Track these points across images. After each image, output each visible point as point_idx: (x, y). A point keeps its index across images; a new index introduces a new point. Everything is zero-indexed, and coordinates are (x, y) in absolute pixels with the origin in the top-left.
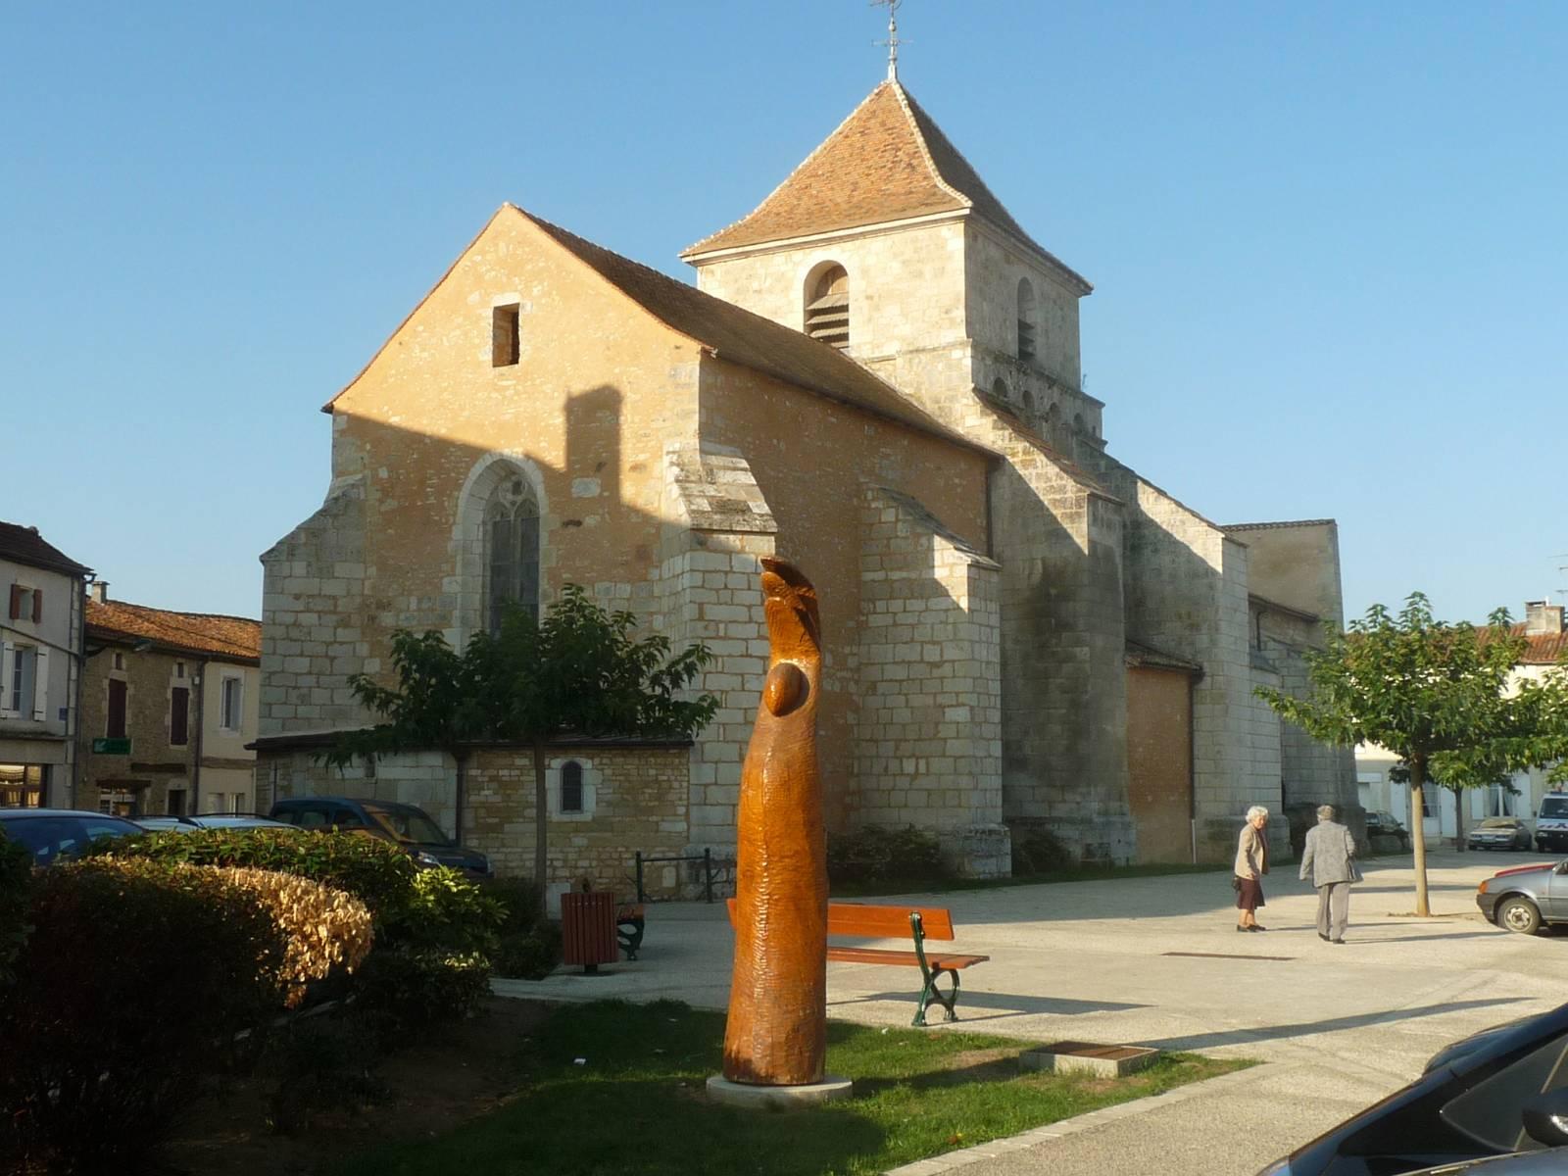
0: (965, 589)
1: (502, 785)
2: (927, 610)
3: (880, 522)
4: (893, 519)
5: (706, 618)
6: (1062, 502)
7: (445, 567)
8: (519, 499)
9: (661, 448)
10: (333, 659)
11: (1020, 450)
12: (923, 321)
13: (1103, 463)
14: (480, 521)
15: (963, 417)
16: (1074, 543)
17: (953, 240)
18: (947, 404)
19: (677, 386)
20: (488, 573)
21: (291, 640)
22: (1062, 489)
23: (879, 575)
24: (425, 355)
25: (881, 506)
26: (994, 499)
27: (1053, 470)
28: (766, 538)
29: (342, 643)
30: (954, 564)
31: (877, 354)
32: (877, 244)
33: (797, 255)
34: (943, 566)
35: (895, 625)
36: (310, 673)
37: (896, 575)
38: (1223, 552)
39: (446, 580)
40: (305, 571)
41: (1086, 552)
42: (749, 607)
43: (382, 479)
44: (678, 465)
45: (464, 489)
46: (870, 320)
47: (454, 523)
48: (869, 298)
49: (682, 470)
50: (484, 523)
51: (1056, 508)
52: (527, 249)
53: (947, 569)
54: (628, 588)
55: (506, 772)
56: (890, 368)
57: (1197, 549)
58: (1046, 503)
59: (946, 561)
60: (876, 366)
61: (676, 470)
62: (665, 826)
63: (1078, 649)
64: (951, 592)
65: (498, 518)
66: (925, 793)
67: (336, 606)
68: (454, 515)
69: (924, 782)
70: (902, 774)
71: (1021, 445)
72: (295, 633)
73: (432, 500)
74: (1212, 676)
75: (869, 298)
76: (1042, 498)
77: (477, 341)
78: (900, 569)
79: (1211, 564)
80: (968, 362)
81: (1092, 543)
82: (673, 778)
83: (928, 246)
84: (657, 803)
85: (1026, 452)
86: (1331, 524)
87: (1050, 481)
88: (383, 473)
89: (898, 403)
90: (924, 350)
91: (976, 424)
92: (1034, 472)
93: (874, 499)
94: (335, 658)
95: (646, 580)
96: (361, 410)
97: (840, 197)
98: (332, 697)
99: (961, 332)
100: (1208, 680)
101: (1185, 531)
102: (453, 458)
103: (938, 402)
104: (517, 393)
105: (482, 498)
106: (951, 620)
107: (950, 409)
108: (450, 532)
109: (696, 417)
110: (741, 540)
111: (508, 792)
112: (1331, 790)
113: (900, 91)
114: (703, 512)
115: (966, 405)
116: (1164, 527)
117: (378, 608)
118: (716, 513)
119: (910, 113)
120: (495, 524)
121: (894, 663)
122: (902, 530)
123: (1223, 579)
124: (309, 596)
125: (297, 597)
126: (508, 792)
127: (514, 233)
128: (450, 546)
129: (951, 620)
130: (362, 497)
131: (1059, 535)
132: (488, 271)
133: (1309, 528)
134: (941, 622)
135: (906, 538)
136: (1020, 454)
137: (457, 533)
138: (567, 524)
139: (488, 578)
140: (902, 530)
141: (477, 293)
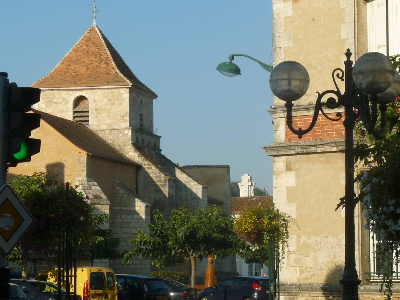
2: (133, 218)
3: (119, 193)
4: (123, 193)
6: (160, 181)
9: (75, 179)
11: (147, 164)
12: (115, 119)
13: (163, 160)
15: (128, 152)
16: (164, 194)
17: (125, 95)
18: (123, 147)
19: (80, 163)
22: (160, 177)
23: (119, 208)
26: (138, 178)
27: (157, 171)
28: (107, 205)
30: (141, 206)
32: (99, 92)
33: (71, 92)
34: (138, 206)
35: (123, 222)
37: (123, 208)
38: (202, 191)
41: (167, 196)
46: (96, 117)
48: (96, 110)
49: (83, 186)
51: (158, 183)
53: (139, 207)
56: (103, 133)
57: (194, 191)
58: (155, 181)
59: (138, 205)
60: (99, 132)
71: (147, 162)
75: (96, 110)
76: (153, 179)
78: (124, 207)
79: (198, 195)
80: (130, 134)
81: (169, 194)
83: (116, 95)
85: (149, 165)
86: (228, 167)
89: (126, 159)
90: (115, 129)
91: (132, 154)
92: (151, 171)
93: (117, 186)
97: (83, 71)
99: (128, 125)
101: (190, 184)
103: (120, 146)
107: (124, 148)
109: (86, 172)
110: (101, 206)
112: (228, 267)
113: (99, 31)
114: (92, 199)
115: (129, 148)
116: (183, 182)
118: (95, 199)
119: (104, 41)
121: (122, 233)
122: (125, 196)
123: (202, 200)
129: (140, 222)
131: (160, 191)
134: (137, 222)
136: (147, 165)
140: (125, 196)
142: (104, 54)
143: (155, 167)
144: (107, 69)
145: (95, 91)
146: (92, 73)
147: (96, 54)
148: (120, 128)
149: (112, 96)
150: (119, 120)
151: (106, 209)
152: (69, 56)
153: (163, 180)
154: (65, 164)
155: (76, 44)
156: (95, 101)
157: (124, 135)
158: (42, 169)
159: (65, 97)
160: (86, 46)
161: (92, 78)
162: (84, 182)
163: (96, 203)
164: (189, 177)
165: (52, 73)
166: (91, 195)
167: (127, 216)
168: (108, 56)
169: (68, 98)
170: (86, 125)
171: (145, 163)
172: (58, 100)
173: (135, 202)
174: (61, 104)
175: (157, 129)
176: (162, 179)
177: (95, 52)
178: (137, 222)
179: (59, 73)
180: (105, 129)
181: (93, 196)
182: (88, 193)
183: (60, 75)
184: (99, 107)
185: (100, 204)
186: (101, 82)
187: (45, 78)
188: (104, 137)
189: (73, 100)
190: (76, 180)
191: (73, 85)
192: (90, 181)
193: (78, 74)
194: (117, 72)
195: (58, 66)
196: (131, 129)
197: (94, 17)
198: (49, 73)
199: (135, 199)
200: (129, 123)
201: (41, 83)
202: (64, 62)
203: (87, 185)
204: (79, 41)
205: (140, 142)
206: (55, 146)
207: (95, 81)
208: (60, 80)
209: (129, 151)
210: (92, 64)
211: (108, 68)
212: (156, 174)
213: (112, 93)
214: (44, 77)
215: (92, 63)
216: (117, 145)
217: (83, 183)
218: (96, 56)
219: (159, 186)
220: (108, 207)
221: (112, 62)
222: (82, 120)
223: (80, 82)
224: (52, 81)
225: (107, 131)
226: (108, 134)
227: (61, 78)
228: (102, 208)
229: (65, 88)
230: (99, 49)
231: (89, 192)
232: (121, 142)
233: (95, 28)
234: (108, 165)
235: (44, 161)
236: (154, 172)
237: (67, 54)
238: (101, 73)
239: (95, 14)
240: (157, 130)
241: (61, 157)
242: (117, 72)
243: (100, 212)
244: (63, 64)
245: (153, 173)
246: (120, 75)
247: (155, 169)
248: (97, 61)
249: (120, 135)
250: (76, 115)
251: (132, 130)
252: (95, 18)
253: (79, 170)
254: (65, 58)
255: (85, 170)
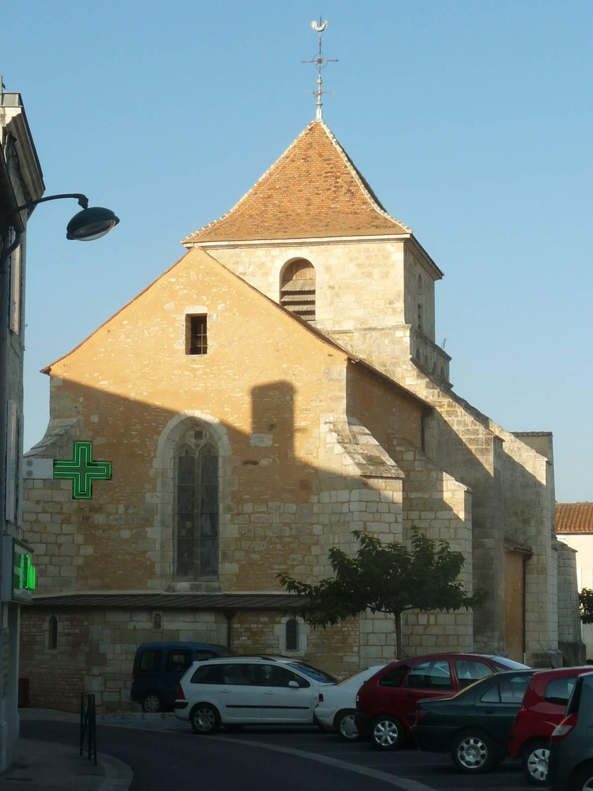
0: (462, 506)
1: (253, 634)
2: (436, 518)
4: (412, 459)
5: (368, 530)
7: (147, 486)
8: (202, 442)
9: (318, 419)
10: (60, 545)
12: (373, 308)
14: (171, 456)
16: (484, 469)
18: (391, 368)
20: (177, 491)
21: (34, 532)
22: (476, 432)
24: (129, 340)
25: (404, 450)
28: (398, 481)
29: (66, 534)
30: (455, 490)
31: (337, 328)
33: (275, 251)
34: (448, 491)
36: (45, 555)
39: (148, 495)
40: (42, 485)
41: (492, 475)
42: (389, 523)
43: (93, 423)
44: (335, 432)
45: (162, 434)
46: (332, 303)
47: (155, 456)
49: (339, 435)
50: (174, 457)
52: (213, 279)
54: (294, 507)
55: (254, 626)
57: (529, 468)
58: (464, 440)
59: (449, 488)
60: (337, 336)
61: (335, 435)
62: (346, 659)
63: (486, 540)
64: (454, 508)
65: (183, 454)
66: (435, 637)
67: (61, 508)
68: (155, 450)
69: (434, 630)
70: (418, 625)
72: (36, 528)
73: (136, 440)
74: (538, 555)
76: (461, 437)
77: (172, 335)
78: (417, 491)
79: (539, 478)
80: (407, 340)
82: (350, 629)
83: (376, 256)
84: (341, 645)
85: (449, 405)
86: (550, 435)
87: (467, 425)
88: (95, 419)
92: (456, 419)
93: (398, 445)
94: (62, 544)
95: (307, 502)
96: (67, 375)
97: (300, 208)
98: (60, 571)
99: (401, 318)
100: (535, 558)
101: (520, 455)
102: (153, 413)
103: (385, 366)
104: (205, 373)
105: (174, 441)
106: (452, 526)
108: (151, 462)
109: (345, 401)
110: (385, 482)
111: (257, 638)
114: (364, 464)
115: (407, 370)
117: (90, 511)
118: (370, 465)
120: (180, 459)
124: (45, 502)
125: (38, 502)
126: (257, 638)
127: (202, 267)
128: (152, 472)
130: (78, 434)
132: (181, 289)
133: (534, 438)
134: (446, 527)
135: (422, 471)
136: (446, 406)
137: (157, 463)
138: (246, 463)
139: (177, 494)
141: (172, 303)
142: (343, 174)
143: (463, 411)
144: (352, 203)
145: (329, 247)
146: (319, 213)
147: (325, 175)
148: (384, 327)
149: (367, 258)
150: (383, 310)
151: (397, 491)
152: (267, 179)
153: (482, 438)
154: (294, 382)
155: (282, 156)
156: (328, 269)
157: (393, 342)
158: (237, 395)
159: (263, 260)
160: (303, 159)
161: (321, 221)
162: (341, 425)
163: (373, 475)
164: (517, 440)
165: (232, 214)
166: (360, 457)
167: (423, 513)
168: (353, 178)
169: (269, 264)
170: (308, 322)
171: (441, 402)
172: (248, 268)
173: (442, 480)
174: (254, 276)
175: (445, 340)
176: (481, 436)
177: (325, 171)
178: (446, 527)
179: (247, 213)
180: (352, 329)
181: (364, 459)
182: (352, 451)
183: (251, 216)
184: (338, 282)
185: (381, 477)
186: (341, 228)
187: (218, 223)
188: (349, 347)
189: (280, 268)
190: (322, 420)
191: (280, 234)
192: (354, 425)
193: (290, 215)
194: (373, 210)
195: (245, 199)
196: (410, 328)
197: (319, 103)
198: (227, 214)
199: (442, 474)
200: (403, 316)
201: (210, 233)
202: (258, 192)
203: (348, 432)
204: (289, 151)
205: (422, 359)
206: (271, 341)
207: (327, 226)
208: (252, 225)
209: (404, 376)
210: (320, 194)
211: (353, 202)
212: (467, 425)
213: (368, 250)
214: (216, 221)
215: (319, 192)
216: (378, 363)
217: (340, 429)
218: (327, 179)
219: (473, 452)
220: (399, 484)
221: (362, 190)
222: (301, 310)
223: (295, 228)
224: (234, 229)
225: (355, 334)
226: (359, 340)
227: (253, 222)
228: (386, 487)
229: (263, 242)
230: (331, 166)
231: (354, 450)
232: (387, 356)
233: (322, 124)
234: (380, 393)
235: (243, 375)
236: (461, 421)
237: (264, 175)
238: (339, 212)
239: (319, 96)
240: (446, 342)
241: (284, 366)
242: (375, 208)
243: (381, 497)
244: (256, 196)
245: (459, 422)
246: (382, 216)
247: (465, 416)
248: (330, 189)
249: (384, 341)
250: (286, 300)
251: (410, 330)
252: (321, 105)
253: (329, 396)
254: (259, 184)
255: (342, 398)
